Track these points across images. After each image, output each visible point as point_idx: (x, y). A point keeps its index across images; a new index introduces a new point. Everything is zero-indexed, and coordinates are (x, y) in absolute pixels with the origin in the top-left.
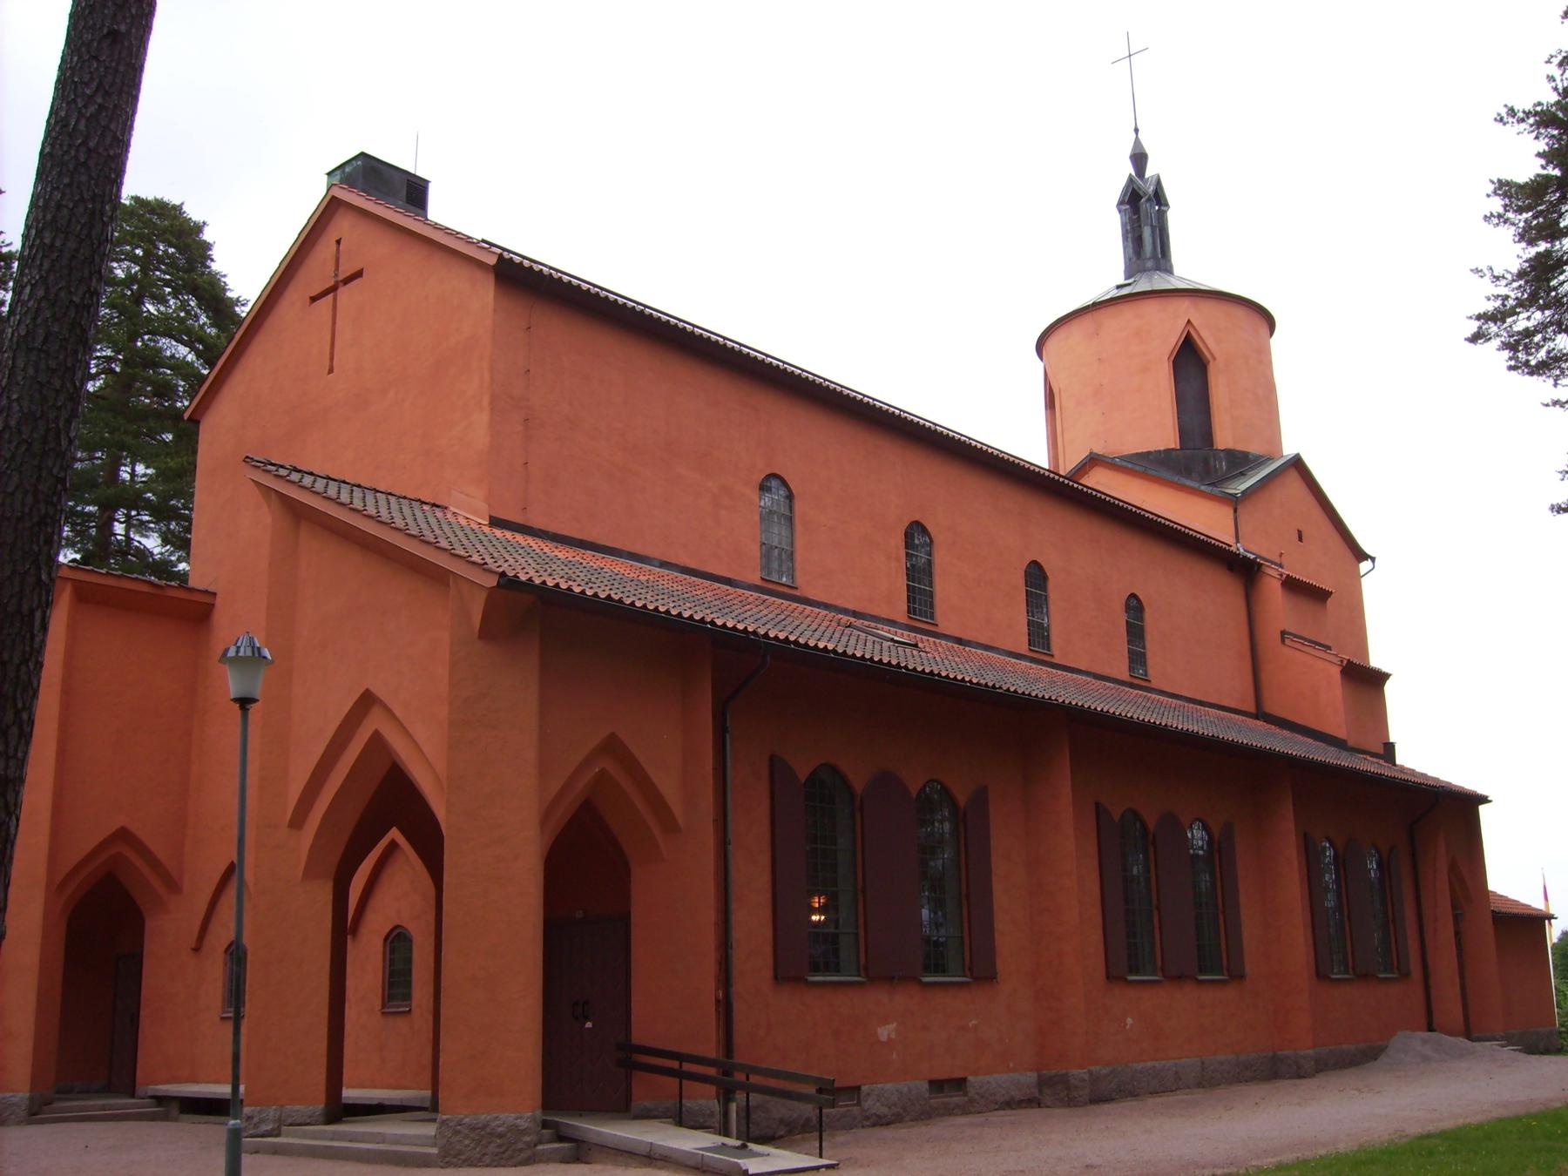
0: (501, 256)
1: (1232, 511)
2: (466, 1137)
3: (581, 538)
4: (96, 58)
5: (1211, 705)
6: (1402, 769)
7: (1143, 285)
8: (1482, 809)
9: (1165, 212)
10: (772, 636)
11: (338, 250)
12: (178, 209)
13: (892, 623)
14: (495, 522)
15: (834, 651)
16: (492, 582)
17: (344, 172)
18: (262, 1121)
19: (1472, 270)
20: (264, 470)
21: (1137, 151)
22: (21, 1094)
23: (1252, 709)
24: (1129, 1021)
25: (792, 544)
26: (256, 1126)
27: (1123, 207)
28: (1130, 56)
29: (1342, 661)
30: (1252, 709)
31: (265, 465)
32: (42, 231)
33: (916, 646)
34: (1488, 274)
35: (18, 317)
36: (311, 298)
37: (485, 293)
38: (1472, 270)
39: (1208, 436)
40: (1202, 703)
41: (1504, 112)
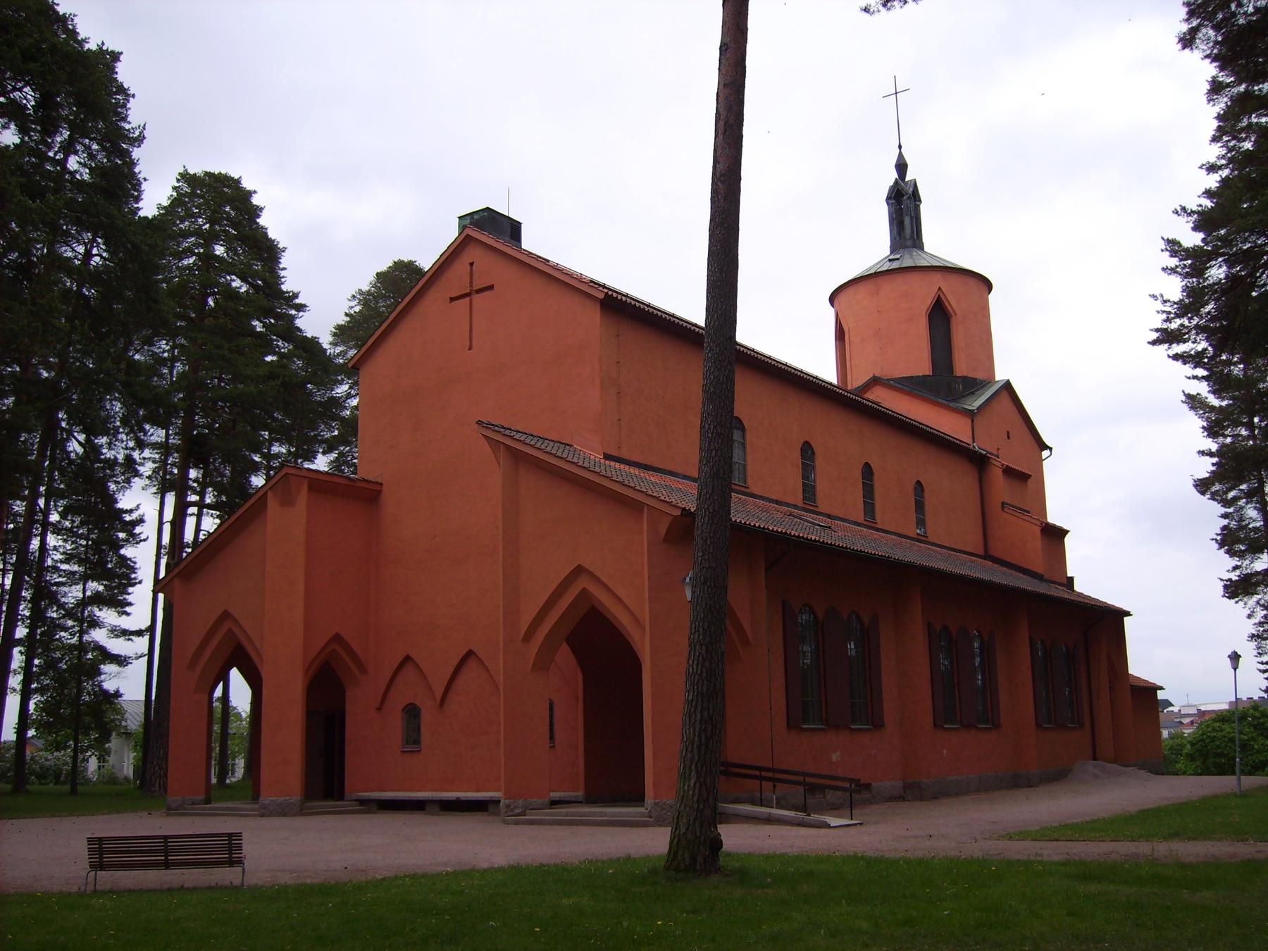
0: (607, 293)
1: (970, 421)
2: (668, 811)
3: (645, 463)
4: (726, 349)
5: (960, 551)
6: (1080, 595)
7: (908, 262)
8: (1126, 619)
9: (919, 206)
10: (793, 534)
11: (471, 270)
12: (237, 182)
13: (795, 507)
14: (607, 457)
15: (819, 541)
16: (678, 513)
17: (473, 218)
18: (516, 807)
19: (1150, 296)
20: (493, 430)
21: (901, 162)
22: (294, 798)
23: (981, 552)
24: (945, 752)
25: (745, 461)
26: (512, 810)
27: (891, 202)
28: (896, 93)
29: (1041, 524)
30: (981, 552)
31: (490, 426)
32: (716, 427)
33: (829, 527)
34: (1160, 299)
35: (712, 464)
36: (450, 298)
37: (594, 315)
38: (1150, 296)
39: (950, 367)
40: (955, 550)
41: (1179, 209)
